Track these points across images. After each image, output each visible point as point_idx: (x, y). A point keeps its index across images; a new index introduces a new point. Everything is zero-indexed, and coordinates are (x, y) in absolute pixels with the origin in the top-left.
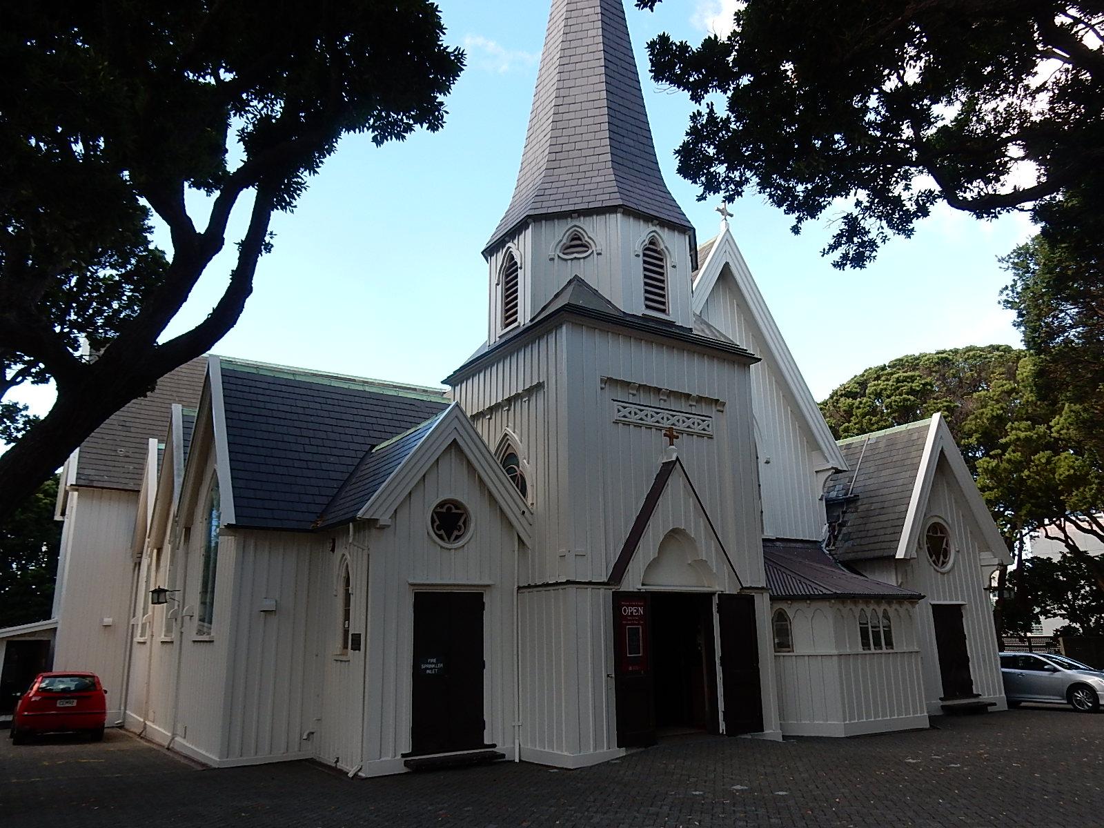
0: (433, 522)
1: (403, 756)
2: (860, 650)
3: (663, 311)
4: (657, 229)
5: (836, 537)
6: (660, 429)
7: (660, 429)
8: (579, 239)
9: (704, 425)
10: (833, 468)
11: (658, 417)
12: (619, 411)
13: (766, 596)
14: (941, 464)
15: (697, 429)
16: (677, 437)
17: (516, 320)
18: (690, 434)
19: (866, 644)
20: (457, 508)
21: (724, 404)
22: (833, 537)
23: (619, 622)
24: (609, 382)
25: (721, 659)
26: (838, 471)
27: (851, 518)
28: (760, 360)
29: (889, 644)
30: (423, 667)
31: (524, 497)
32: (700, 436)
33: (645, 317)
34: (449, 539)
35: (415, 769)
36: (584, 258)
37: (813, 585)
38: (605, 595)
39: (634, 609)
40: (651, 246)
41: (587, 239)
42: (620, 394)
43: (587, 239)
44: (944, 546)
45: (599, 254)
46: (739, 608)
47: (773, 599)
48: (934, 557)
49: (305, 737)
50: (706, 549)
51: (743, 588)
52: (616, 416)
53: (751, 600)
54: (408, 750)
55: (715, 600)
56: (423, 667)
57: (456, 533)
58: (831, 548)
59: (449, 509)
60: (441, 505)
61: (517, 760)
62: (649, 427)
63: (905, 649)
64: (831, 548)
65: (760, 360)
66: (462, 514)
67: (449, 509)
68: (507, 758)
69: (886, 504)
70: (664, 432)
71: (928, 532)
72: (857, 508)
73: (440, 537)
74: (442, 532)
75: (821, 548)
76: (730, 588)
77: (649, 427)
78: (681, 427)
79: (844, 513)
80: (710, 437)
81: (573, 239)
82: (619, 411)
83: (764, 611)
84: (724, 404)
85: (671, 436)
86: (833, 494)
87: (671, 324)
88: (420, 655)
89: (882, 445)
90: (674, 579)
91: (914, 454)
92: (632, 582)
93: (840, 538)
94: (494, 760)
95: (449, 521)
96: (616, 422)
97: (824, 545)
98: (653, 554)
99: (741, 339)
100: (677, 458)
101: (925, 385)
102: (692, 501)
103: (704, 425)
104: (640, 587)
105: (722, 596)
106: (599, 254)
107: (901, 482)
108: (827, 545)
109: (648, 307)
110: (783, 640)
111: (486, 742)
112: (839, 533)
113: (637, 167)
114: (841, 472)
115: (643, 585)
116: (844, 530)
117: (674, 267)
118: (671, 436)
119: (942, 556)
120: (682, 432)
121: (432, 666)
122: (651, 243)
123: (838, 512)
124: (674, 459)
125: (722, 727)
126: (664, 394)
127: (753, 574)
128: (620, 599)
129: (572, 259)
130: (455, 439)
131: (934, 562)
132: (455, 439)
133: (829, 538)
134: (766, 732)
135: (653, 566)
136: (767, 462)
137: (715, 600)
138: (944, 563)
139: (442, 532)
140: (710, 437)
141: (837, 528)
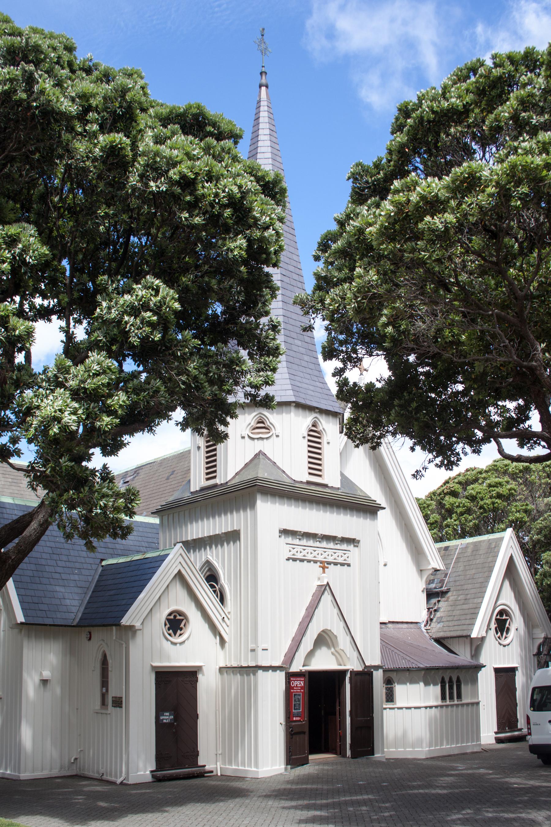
0: (165, 625)
1: (152, 772)
2: (440, 703)
3: (320, 476)
4: (318, 415)
5: (431, 620)
6: (315, 562)
7: (315, 562)
8: (263, 422)
9: (345, 557)
10: (433, 568)
11: (315, 554)
12: (290, 551)
13: (381, 671)
14: (511, 564)
15: (340, 560)
16: (327, 568)
17: (215, 477)
18: (336, 564)
19: (443, 698)
20: (180, 615)
21: (358, 542)
22: (430, 620)
23: (289, 689)
24: (285, 532)
25: (351, 712)
26: (436, 570)
27: (443, 605)
28: (384, 508)
29: (459, 697)
30: (161, 718)
31: (223, 604)
32: (342, 565)
33: (308, 483)
34: (175, 635)
35: (157, 779)
36: (267, 438)
37: (412, 661)
38: (281, 676)
39: (298, 683)
40: (314, 428)
41: (269, 424)
42: (290, 540)
43: (269, 424)
44: (507, 625)
45: (277, 436)
46: (363, 679)
47: (385, 671)
48: (499, 634)
49: (72, 761)
50: (343, 641)
51: (366, 667)
52: (290, 555)
53: (370, 675)
54: (154, 769)
55: (348, 675)
56: (161, 718)
57: (179, 632)
58: (428, 627)
59: (175, 616)
60: (170, 614)
61: (219, 774)
62: (309, 561)
63: (469, 701)
64: (428, 627)
65: (384, 508)
66: (183, 620)
67: (175, 616)
68: (214, 773)
69: (469, 597)
70: (319, 563)
71: (497, 615)
72: (448, 598)
73: (170, 635)
74: (171, 631)
75: (420, 628)
76: (359, 668)
77: (309, 561)
78: (330, 559)
79: (439, 601)
80: (349, 565)
81: (259, 422)
82: (290, 551)
83: (378, 676)
84: (358, 542)
85: (324, 565)
86: (433, 586)
87: (325, 486)
88: (160, 709)
89: (469, 550)
90: (324, 662)
91: (490, 559)
92: (297, 667)
93: (434, 620)
94: (202, 774)
95: (176, 623)
96: (288, 559)
97: (423, 625)
98: (310, 647)
99: (373, 491)
100: (328, 583)
101: (510, 490)
102: (336, 611)
103: (345, 557)
104: (301, 668)
105: (355, 674)
106: (277, 436)
107: (480, 580)
108: (425, 626)
109: (310, 474)
110: (390, 697)
111: (200, 763)
112: (434, 617)
113: (304, 364)
114: (438, 570)
115: (303, 666)
116: (438, 614)
117: (328, 443)
118: (324, 565)
119: (505, 633)
120: (329, 563)
121: (167, 717)
122: (313, 426)
123: (434, 601)
124: (325, 583)
125: (349, 753)
126: (319, 538)
127: (373, 658)
128: (290, 676)
129: (258, 439)
130: (179, 572)
131: (499, 638)
132: (179, 572)
133: (427, 622)
134: (376, 755)
135: (311, 654)
136: (385, 565)
137: (348, 675)
138: (506, 638)
139: (171, 631)
140: (349, 565)
141: (433, 613)
